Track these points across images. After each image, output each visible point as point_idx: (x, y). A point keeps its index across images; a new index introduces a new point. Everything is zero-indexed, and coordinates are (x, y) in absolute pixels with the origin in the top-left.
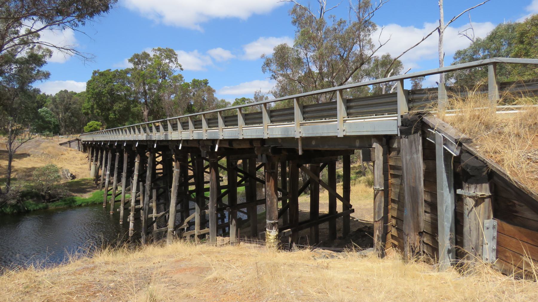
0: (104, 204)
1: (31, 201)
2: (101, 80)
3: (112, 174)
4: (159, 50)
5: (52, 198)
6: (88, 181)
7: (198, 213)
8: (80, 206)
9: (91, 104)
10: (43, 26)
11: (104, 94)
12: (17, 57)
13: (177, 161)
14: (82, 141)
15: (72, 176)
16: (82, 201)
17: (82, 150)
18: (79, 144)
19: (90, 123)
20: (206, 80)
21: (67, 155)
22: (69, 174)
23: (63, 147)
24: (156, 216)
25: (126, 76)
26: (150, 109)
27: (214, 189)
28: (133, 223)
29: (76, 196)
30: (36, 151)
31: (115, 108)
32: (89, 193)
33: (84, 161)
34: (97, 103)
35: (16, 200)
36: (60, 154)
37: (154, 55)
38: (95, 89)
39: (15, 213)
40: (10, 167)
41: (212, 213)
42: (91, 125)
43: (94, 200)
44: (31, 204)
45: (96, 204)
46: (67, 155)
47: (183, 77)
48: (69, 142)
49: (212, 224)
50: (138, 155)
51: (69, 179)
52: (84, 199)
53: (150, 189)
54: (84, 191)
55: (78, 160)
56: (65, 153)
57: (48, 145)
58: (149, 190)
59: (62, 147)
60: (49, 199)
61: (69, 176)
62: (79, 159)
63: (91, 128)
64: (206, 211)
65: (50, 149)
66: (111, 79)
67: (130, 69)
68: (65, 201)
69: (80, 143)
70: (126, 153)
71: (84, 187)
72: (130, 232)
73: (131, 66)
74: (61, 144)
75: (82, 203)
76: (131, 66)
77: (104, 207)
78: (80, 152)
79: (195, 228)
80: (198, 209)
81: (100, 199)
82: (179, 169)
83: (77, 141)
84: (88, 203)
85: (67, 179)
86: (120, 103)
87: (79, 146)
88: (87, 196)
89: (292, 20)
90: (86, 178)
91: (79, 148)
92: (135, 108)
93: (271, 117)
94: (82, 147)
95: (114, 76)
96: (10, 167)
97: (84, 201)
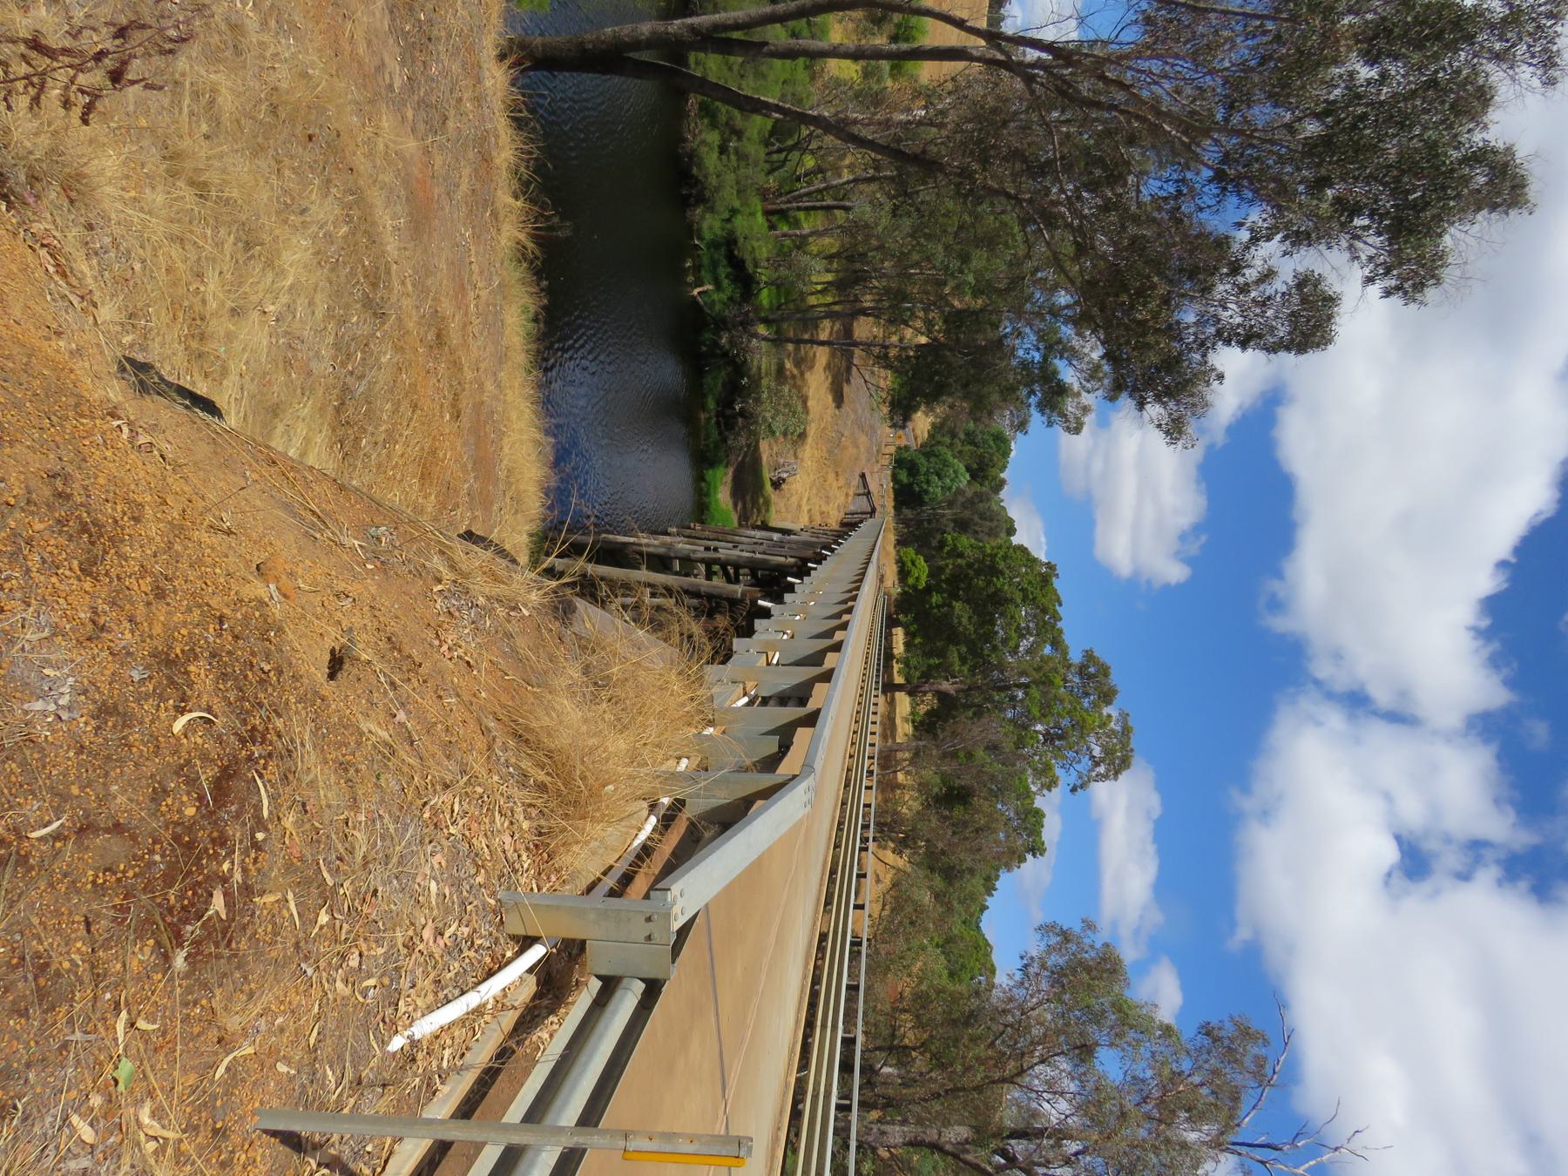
4: (1126, 731)
5: (728, 420)
9: (968, 552)
10: (929, 22)
12: (1057, 362)
18: (862, 513)
19: (921, 561)
20: (1045, 850)
21: (835, 484)
22: (785, 475)
23: (856, 480)
25: (1045, 642)
26: (957, 699)
31: (957, 605)
34: (970, 566)
35: (727, 347)
36: (840, 470)
37: (1109, 716)
42: (917, 562)
44: (716, 381)
45: (702, 514)
47: (1050, 790)
48: (869, 493)
52: (715, 488)
54: (738, 491)
56: (842, 481)
59: (857, 478)
62: (824, 509)
63: (909, 564)
65: (852, 451)
66: (1034, 599)
67: (1065, 653)
68: (717, 447)
73: (1075, 657)
74: (863, 476)
75: (709, 484)
76: (1075, 657)
78: (842, 515)
84: (707, 495)
86: (970, 618)
88: (722, 496)
89: (1214, 1022)
92: (956, 655)
95: (1044, 611)
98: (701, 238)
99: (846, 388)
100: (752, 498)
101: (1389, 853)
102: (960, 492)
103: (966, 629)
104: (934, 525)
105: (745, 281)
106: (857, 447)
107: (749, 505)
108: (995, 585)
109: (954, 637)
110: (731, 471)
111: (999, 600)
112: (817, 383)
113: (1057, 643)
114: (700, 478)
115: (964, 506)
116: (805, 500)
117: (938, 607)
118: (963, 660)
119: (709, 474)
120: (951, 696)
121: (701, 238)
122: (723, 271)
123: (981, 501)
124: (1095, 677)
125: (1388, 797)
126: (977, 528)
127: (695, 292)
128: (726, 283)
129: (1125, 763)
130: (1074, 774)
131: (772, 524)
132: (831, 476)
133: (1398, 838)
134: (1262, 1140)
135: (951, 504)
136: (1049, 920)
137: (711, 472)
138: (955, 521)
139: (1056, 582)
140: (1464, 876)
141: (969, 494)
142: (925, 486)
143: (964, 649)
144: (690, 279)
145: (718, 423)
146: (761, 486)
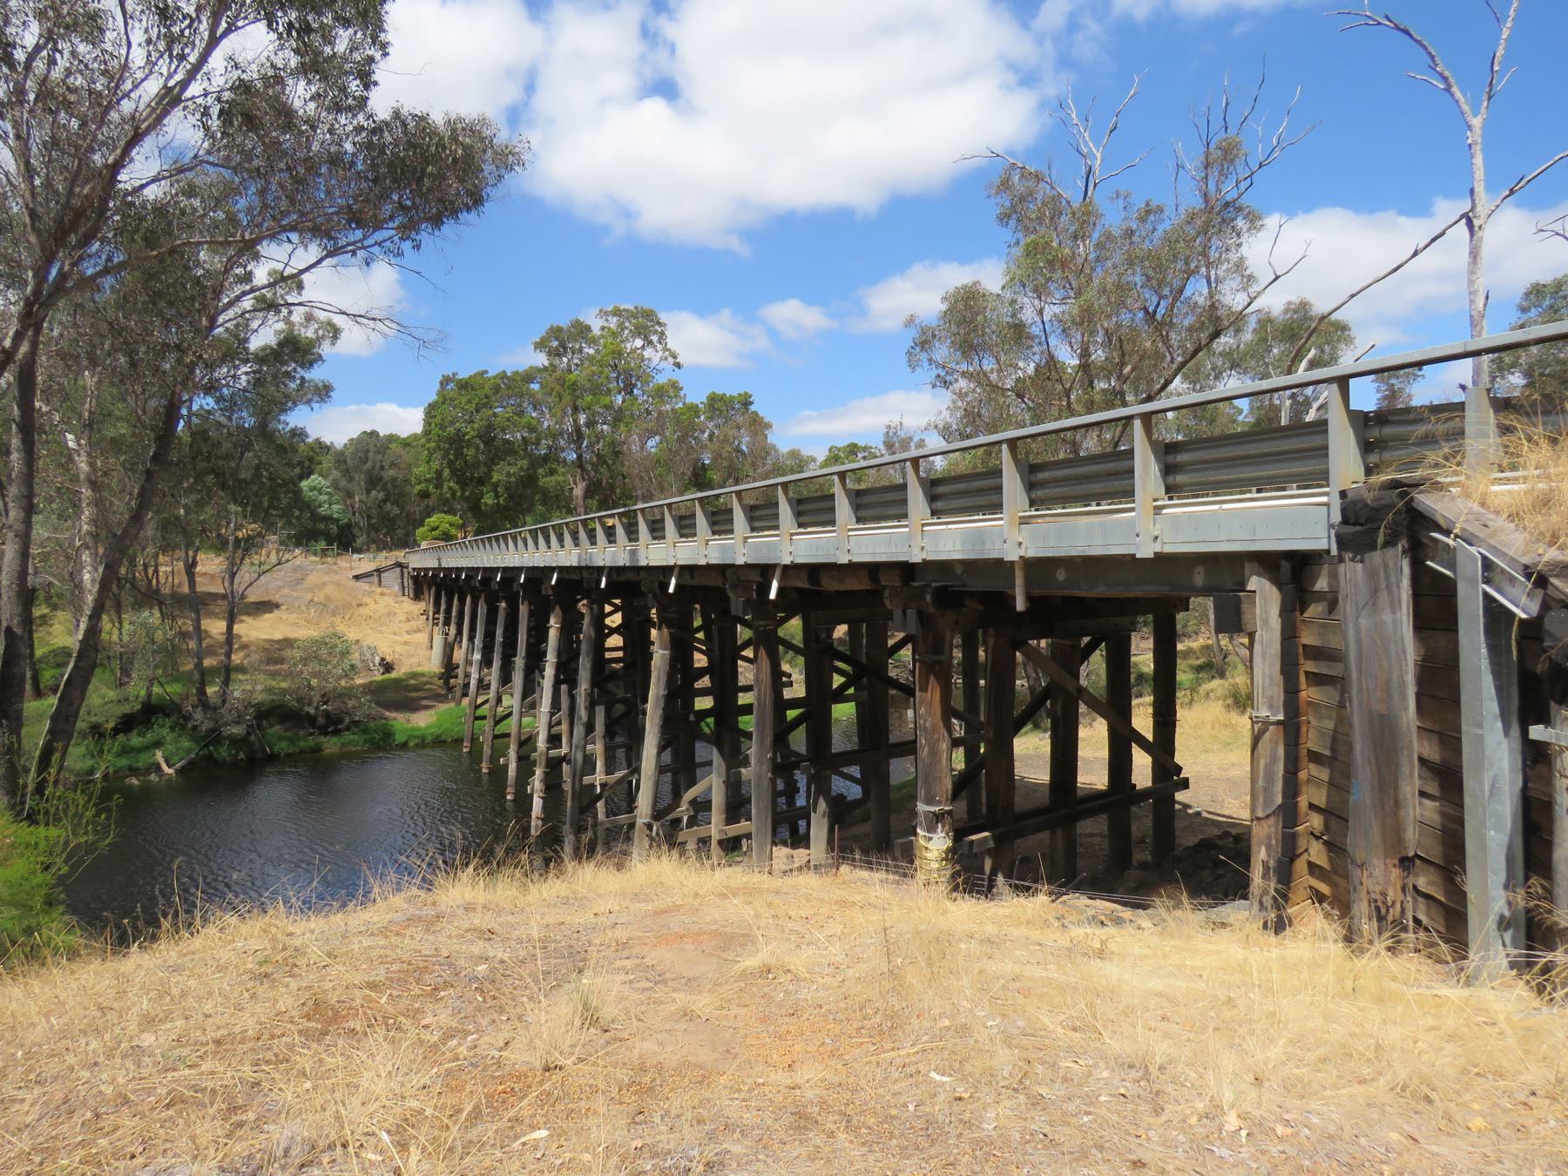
2: (464, 401)
4: (617, 312)
5: (332, 724)
6: (425, 679)
7: (719, 774)
9: (435, 465)
21: (372, 606)
22: (377, 660)
23: (363, 585)
29: (395, 719)
30: (295, 594)
31: (496, 477)
33: (414, 624)
34: (451, 464)
35: (245, 726)
36: (354, 603)
37: (603, 328)
41: (759, 777)
44: (278, 738)
45: (445, 742)
48: (378, 570)
49: (758, 809)
50: (558, 608)
52: (413, 729)
54: (411, 706)
56: (367, 600)
57: (326, 578)
62: (403, 618)
65: (329, 590)
66: (487, 397)
67: (538, 370)
70: (526, 603)
71: (414, 694)
72: (533, 823)
73: (541, 360)
74: (357, 577)
75: (410, 737)
76: (541, 360)
77: (465, 750)
83: (398, 569)
84: (423, 739)
86: (509, 464)
88: (423, 721)
90: (419, 669)
91: (403, 587)
93: (932, 498)
95: (497, 389)
98: (92, 771)
100: (410, 691)
101: (655, 107)
103: (521, 468)
105: (149, 712)
106: (324, 584)
107: (422, 694)
108: (473, 437)
109: (530, 480)
111: (487, 435)
112: (252, 630)
113: (529, 376)
114: (404, 746)
115: (351, 479)
116: (398, 638)
117: (497, 497)
118: (552, 472)
119: (400, 738)
120: (588, 486)
121: (92, 771)
122: (135, 740)
123: (345, 461)
124: (560, 341)
125: (605, 100)
127: (170, 771)
128: (150, 736)
129: (649, 315)
130: (663, 364)
132: (364, 611)
133: (641, 98)
134: (1081, 184)
135: (350, 495)
136: (905, 359)
139: (464, 374)
140: (672, 49)
141: (336, 474)
143: (541, 471)
144: (153, 777)
146: (397, 681)
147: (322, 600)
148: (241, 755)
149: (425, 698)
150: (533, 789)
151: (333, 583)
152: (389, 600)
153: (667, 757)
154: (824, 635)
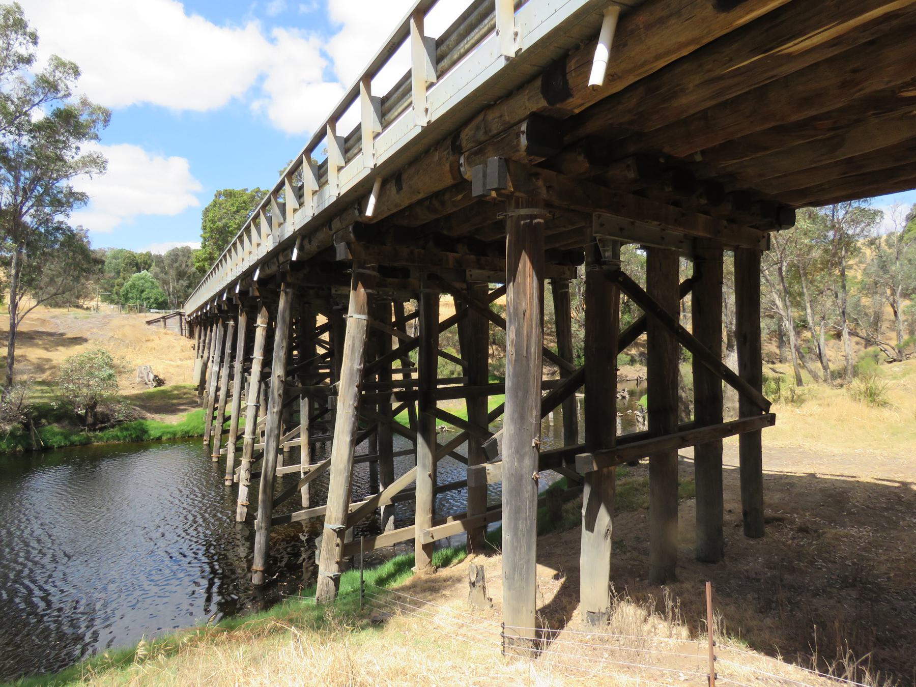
0: (205, 438)
1: (56, 427)
2: (228, 204)
3: (231, 377)
6: (185, 391)
7: (424, 466)
8: (159, 439)
11: (232, 231)
13: (360, 285)
14: (187, 317)
15: (157, 381)
16: (162, 430)
17: (187, 335)
21: (157, 341)
22: (151, 377)
23: (153, 327)
24: (307, 470)
27: (527, 358)
28: (247, 486)
29: (153, 419)
30: (100, 333)
32: (181, 415)
33: (187, 354)
36: (144, 340)
38: (216, 222)
39: (20, 451)
40: (11, 355)
41: (517, 479)
43: (189, 428)
44: (54, 433)
45: (192, 436)
46: (157, 341)
48: (163, 318)
49: (515, 530)
50: (264, 309)
51: (150, 386)
52: (167, 427)
53: (281, 391)
54: (171, 409)
55: (177, 352)
57: (126, 322)
58: (279, 395)
59: (149, 327)
60: (94, 424)
61: (151, 380)
64: (488, 466)
66: (244, 202)
69: (183, 321)
70: (244, 314)
71: (175, 401)
72: (238, 510)
74: (149, 323)
75: (163, 433)
77: (205, 443)
78: (183, 337)
79: (417, 521)
80: (425, 456)
81: (202, 427)
82: (364, 314)
83: (178, 317)
84: (175, 434)
85: (146, 386)
87: (181, 326)
88: (176, 421)
90: (183, 384)
91: (182, 329)
93: (317, 504)
94: (187, 328)
96: (11, 355)
97: (167, 430)
99: (70, 335)
100: (174, 399)
102: (156, 276)
104: (182, 294)
110: (148, 415)
116: (172, 363)
119: (154, 433)
126: (184, 266)
131: (196, 382)
132: (150, 344)
137: (152, 432)
138: (178, 280)
141: (158, 270)
142: (152, 300)
145: (101, 429)
146: (163, 392)
147: (120, 336)
148: (19, 448)
149: (183, 404)
150: (239, 477)
151: (130, 325)
152: (171, 338)
153: (364, 447)
154: (608, 254)
